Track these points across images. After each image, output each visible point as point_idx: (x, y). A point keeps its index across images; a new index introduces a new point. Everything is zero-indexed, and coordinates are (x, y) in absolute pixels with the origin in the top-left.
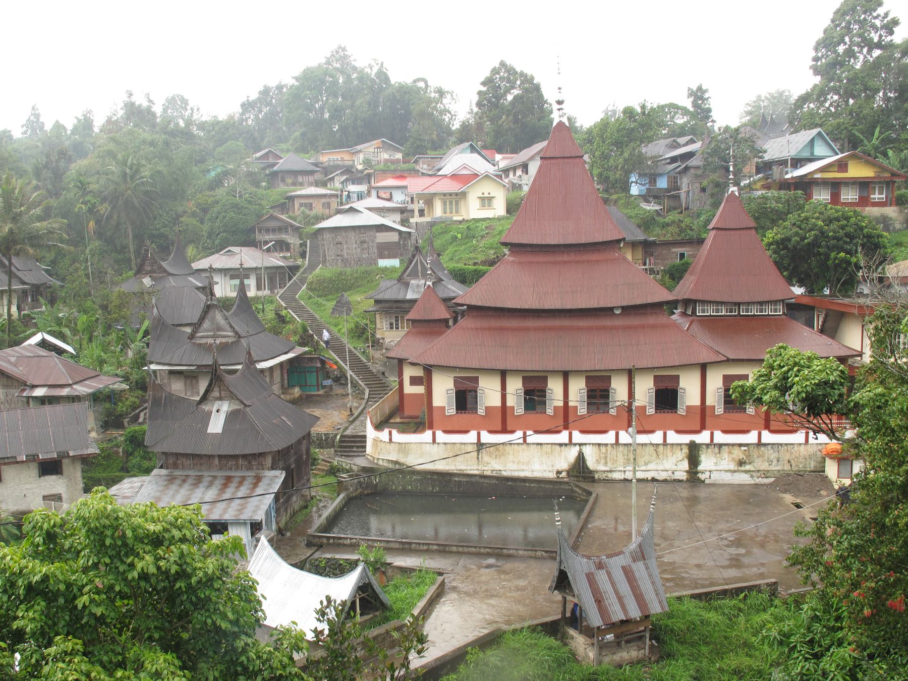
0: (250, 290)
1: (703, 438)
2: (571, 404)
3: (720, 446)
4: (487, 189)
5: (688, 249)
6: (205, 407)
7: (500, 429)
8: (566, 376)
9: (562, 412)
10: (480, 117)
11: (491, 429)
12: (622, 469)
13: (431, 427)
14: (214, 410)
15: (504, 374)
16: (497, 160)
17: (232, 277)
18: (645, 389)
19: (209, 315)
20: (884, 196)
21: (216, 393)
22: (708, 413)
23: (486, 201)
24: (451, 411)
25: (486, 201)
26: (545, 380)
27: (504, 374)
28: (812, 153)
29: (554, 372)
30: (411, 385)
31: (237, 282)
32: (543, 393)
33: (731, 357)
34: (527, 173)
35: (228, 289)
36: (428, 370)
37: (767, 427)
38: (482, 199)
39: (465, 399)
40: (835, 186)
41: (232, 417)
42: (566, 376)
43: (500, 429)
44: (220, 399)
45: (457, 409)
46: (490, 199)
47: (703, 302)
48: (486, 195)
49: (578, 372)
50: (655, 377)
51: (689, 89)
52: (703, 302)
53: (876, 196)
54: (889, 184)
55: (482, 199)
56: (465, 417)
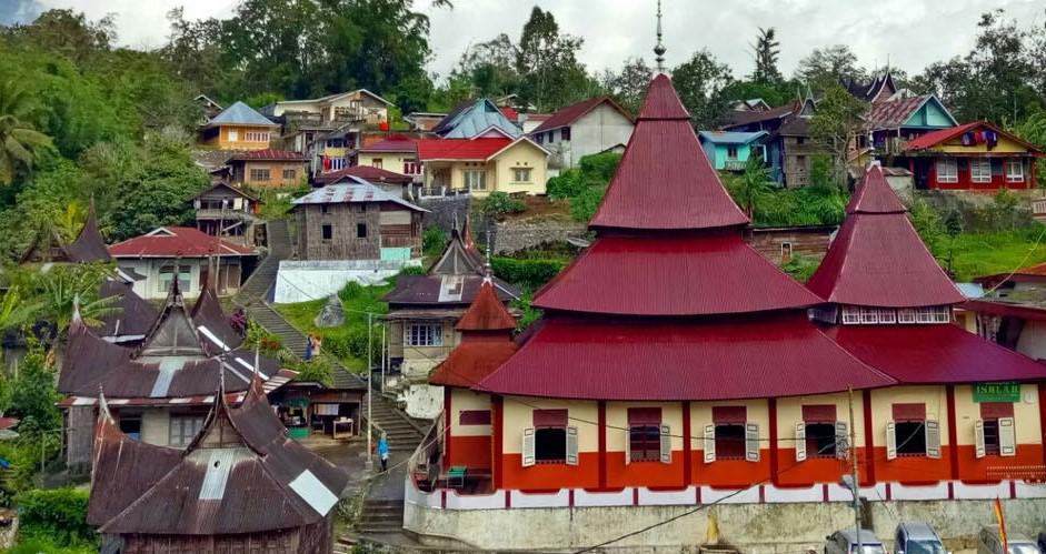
0: (188, 289)
1: (875, 492)
2: (781, 445)
3: (901, 502)
4: (521, 158)
5: (794, 239)
6: (196, 459)
7: (597, 486)
8: (686, 408)
9: (768, 456)
10: (238, 100)
11: (652, 485)
12: (770, 540)
13: (499, 485)
14: (211, 464)
15: (602, 407)
16: (520, 120)
17: (164, 270)
18: (792, 425)
19: (169, 322)
20: (1021, 176)
21: (214, 437)
22: (876, 458)
23: (522, 173)
24: (529, 459)
25: (522, 173)
26: (657, 413)
27: (602, 407)
28: (924, 123)
29: (580, 401)
30: (461, 424)
31: (169, 277)
32: (740, 431)
33: (903, 380)
34: (569, 139)
35: (155, 288)
36: (498, 401)
37: (955, 477)
38: (517, 171)
39: (551, 443)
40: (963, 163)
41: (237, 477)
42: (686, 408)
43: (597, 486)
44: (221, 445)
45: (537, 458)
46: (527, 170)
47: (849, 307)
48: (522, 165)
49: (619, 402)
50: (804, 407)
51: (585, 66)
52: (849, 307)
53: (1013, 176)
54: (1025, 161)
55: (517, 171)
56: (551, 467)
